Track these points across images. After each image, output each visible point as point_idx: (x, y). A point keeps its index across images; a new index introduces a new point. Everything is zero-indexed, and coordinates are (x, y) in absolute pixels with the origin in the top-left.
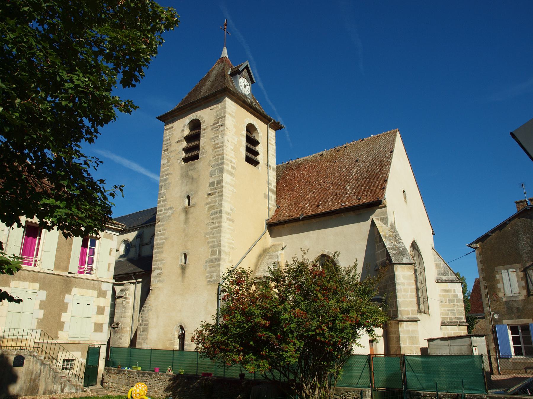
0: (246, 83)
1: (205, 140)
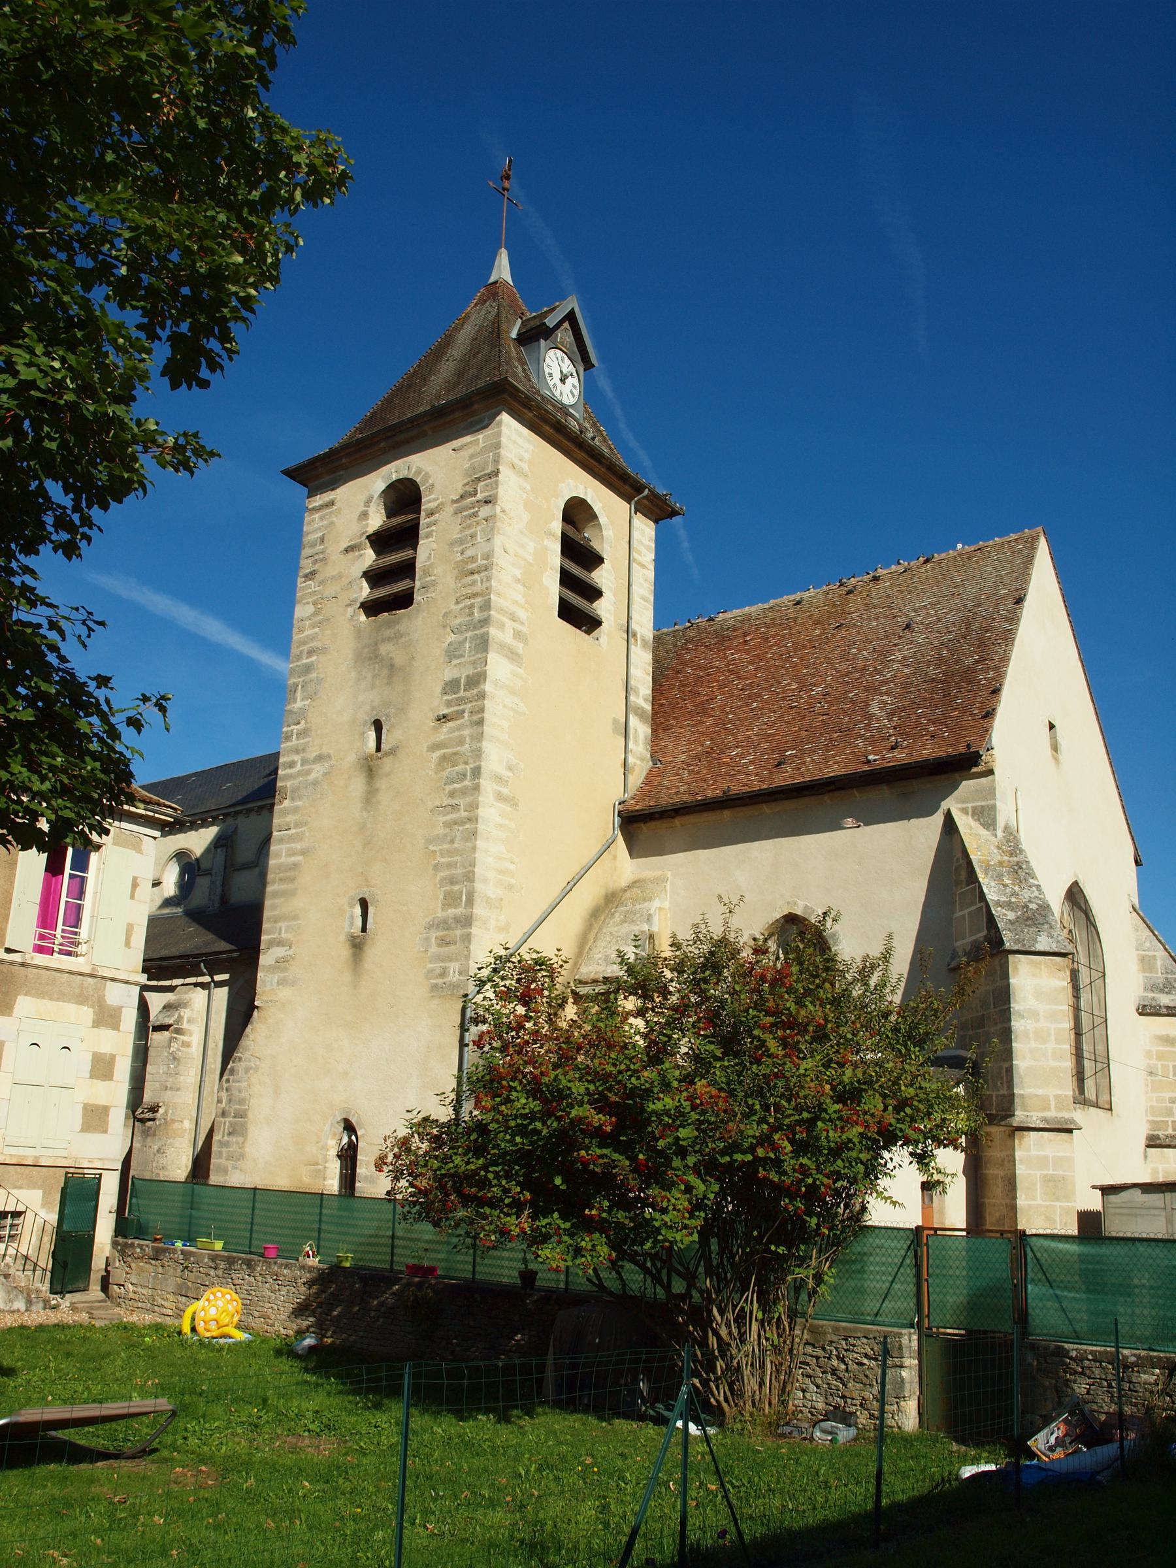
0: (568, 367)
1: (434, 546)
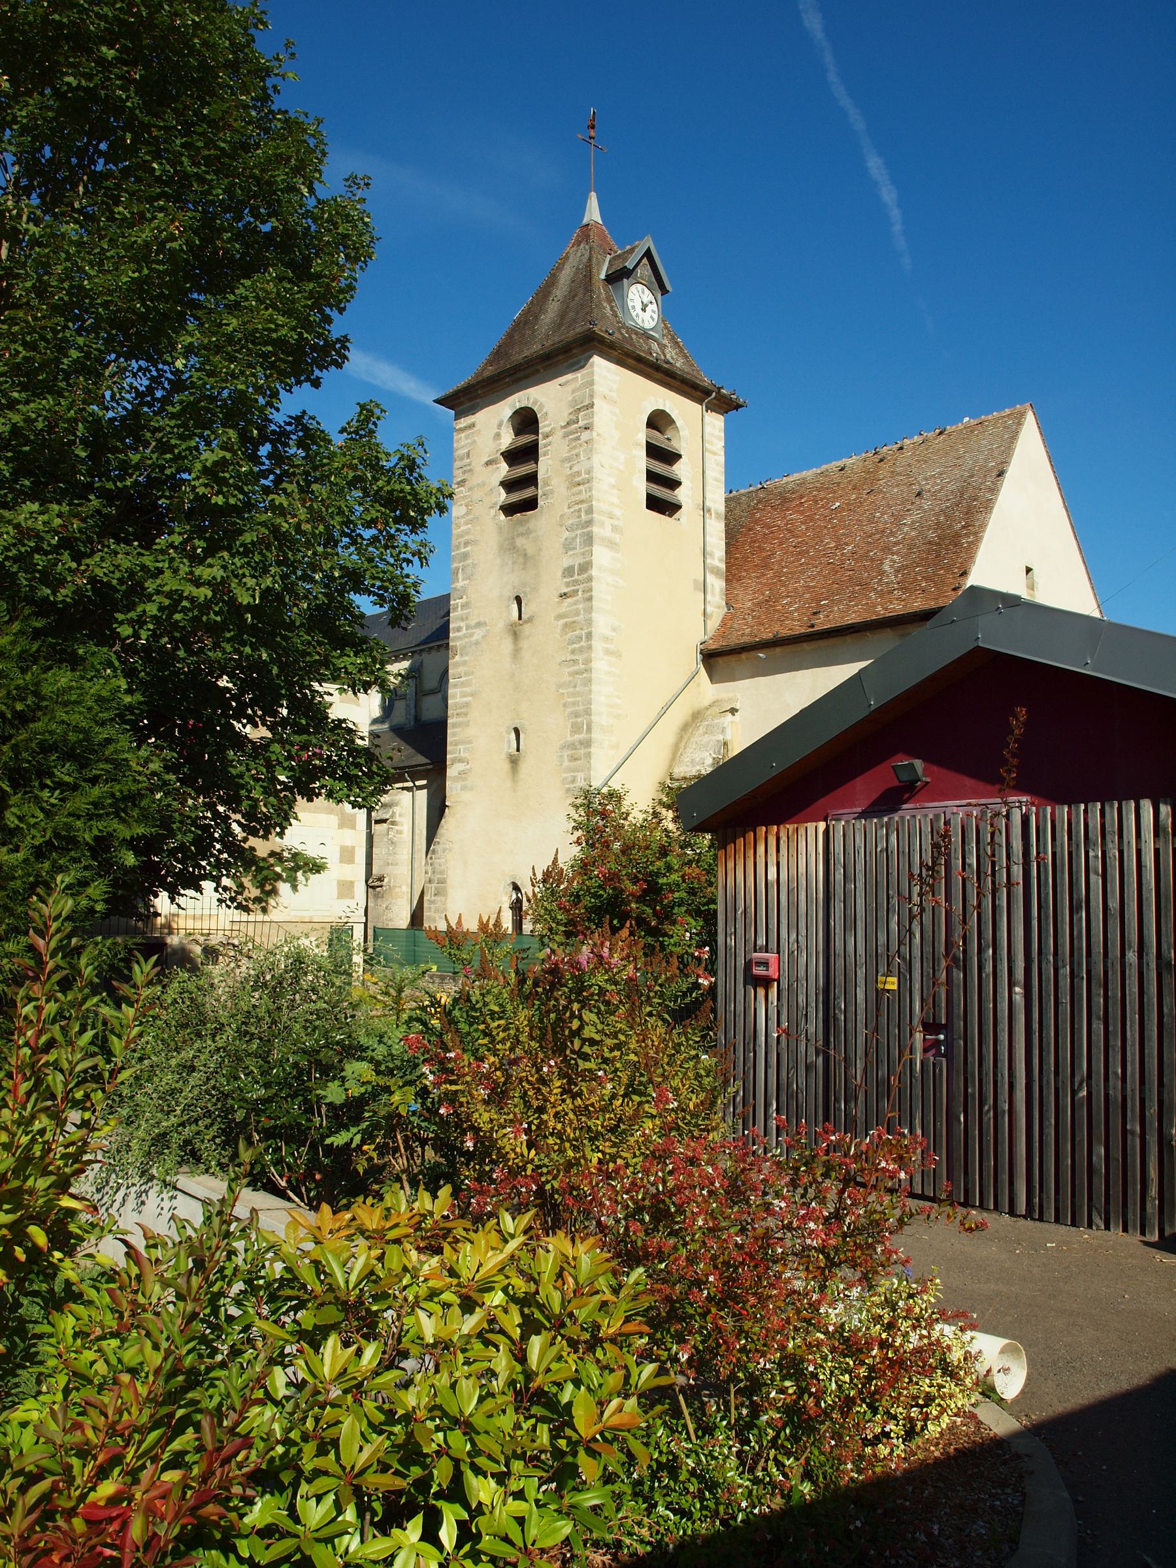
0: (647, 296)
1: (550, 462)
